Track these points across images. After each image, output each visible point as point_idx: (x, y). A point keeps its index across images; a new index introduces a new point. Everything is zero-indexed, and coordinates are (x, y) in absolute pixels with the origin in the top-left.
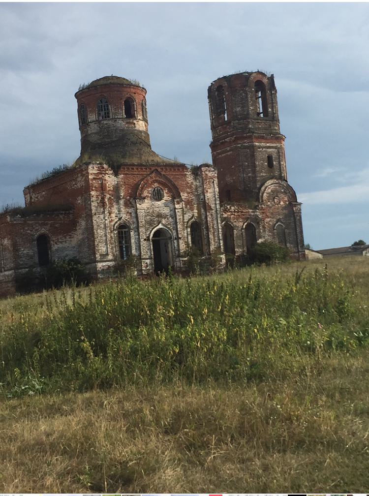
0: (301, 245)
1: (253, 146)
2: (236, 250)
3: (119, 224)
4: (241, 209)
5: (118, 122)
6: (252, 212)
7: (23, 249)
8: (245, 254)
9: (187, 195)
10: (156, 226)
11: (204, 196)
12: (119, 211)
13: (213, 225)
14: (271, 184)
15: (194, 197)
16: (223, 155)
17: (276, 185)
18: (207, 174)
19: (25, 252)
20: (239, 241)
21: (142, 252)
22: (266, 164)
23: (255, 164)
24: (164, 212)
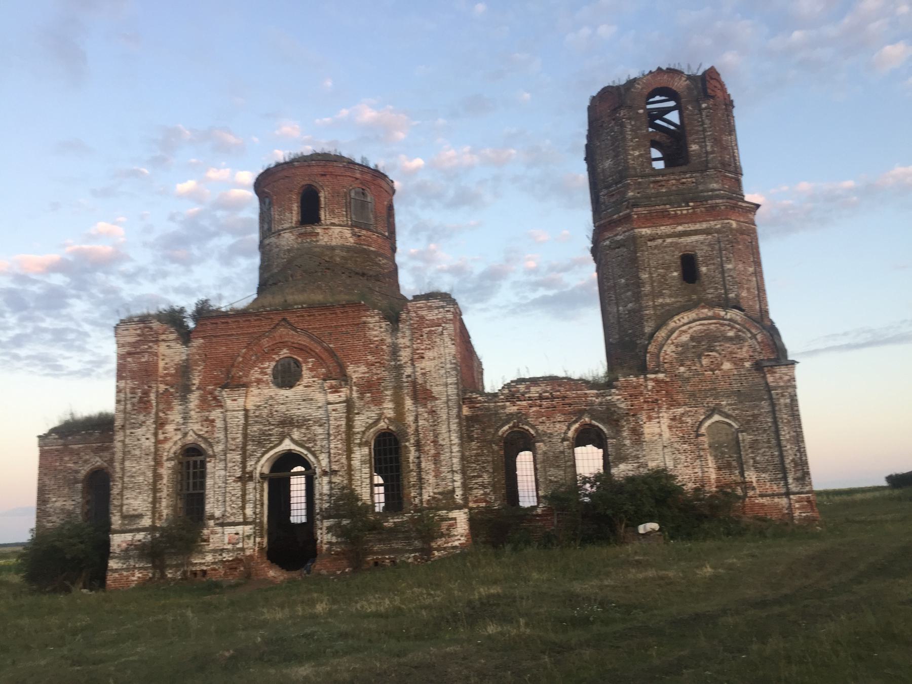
0: (799, 474)
3: (183, 447)
5: (284, 237)
6: (597, 396)
7: (54, 499)
9: (366, 370)
10: (272, 448)
12: (186, 418)
15: (386, 374)
18: (422, 318)
19: (58, 504)
23: (639, 278)
24: (298, 412)
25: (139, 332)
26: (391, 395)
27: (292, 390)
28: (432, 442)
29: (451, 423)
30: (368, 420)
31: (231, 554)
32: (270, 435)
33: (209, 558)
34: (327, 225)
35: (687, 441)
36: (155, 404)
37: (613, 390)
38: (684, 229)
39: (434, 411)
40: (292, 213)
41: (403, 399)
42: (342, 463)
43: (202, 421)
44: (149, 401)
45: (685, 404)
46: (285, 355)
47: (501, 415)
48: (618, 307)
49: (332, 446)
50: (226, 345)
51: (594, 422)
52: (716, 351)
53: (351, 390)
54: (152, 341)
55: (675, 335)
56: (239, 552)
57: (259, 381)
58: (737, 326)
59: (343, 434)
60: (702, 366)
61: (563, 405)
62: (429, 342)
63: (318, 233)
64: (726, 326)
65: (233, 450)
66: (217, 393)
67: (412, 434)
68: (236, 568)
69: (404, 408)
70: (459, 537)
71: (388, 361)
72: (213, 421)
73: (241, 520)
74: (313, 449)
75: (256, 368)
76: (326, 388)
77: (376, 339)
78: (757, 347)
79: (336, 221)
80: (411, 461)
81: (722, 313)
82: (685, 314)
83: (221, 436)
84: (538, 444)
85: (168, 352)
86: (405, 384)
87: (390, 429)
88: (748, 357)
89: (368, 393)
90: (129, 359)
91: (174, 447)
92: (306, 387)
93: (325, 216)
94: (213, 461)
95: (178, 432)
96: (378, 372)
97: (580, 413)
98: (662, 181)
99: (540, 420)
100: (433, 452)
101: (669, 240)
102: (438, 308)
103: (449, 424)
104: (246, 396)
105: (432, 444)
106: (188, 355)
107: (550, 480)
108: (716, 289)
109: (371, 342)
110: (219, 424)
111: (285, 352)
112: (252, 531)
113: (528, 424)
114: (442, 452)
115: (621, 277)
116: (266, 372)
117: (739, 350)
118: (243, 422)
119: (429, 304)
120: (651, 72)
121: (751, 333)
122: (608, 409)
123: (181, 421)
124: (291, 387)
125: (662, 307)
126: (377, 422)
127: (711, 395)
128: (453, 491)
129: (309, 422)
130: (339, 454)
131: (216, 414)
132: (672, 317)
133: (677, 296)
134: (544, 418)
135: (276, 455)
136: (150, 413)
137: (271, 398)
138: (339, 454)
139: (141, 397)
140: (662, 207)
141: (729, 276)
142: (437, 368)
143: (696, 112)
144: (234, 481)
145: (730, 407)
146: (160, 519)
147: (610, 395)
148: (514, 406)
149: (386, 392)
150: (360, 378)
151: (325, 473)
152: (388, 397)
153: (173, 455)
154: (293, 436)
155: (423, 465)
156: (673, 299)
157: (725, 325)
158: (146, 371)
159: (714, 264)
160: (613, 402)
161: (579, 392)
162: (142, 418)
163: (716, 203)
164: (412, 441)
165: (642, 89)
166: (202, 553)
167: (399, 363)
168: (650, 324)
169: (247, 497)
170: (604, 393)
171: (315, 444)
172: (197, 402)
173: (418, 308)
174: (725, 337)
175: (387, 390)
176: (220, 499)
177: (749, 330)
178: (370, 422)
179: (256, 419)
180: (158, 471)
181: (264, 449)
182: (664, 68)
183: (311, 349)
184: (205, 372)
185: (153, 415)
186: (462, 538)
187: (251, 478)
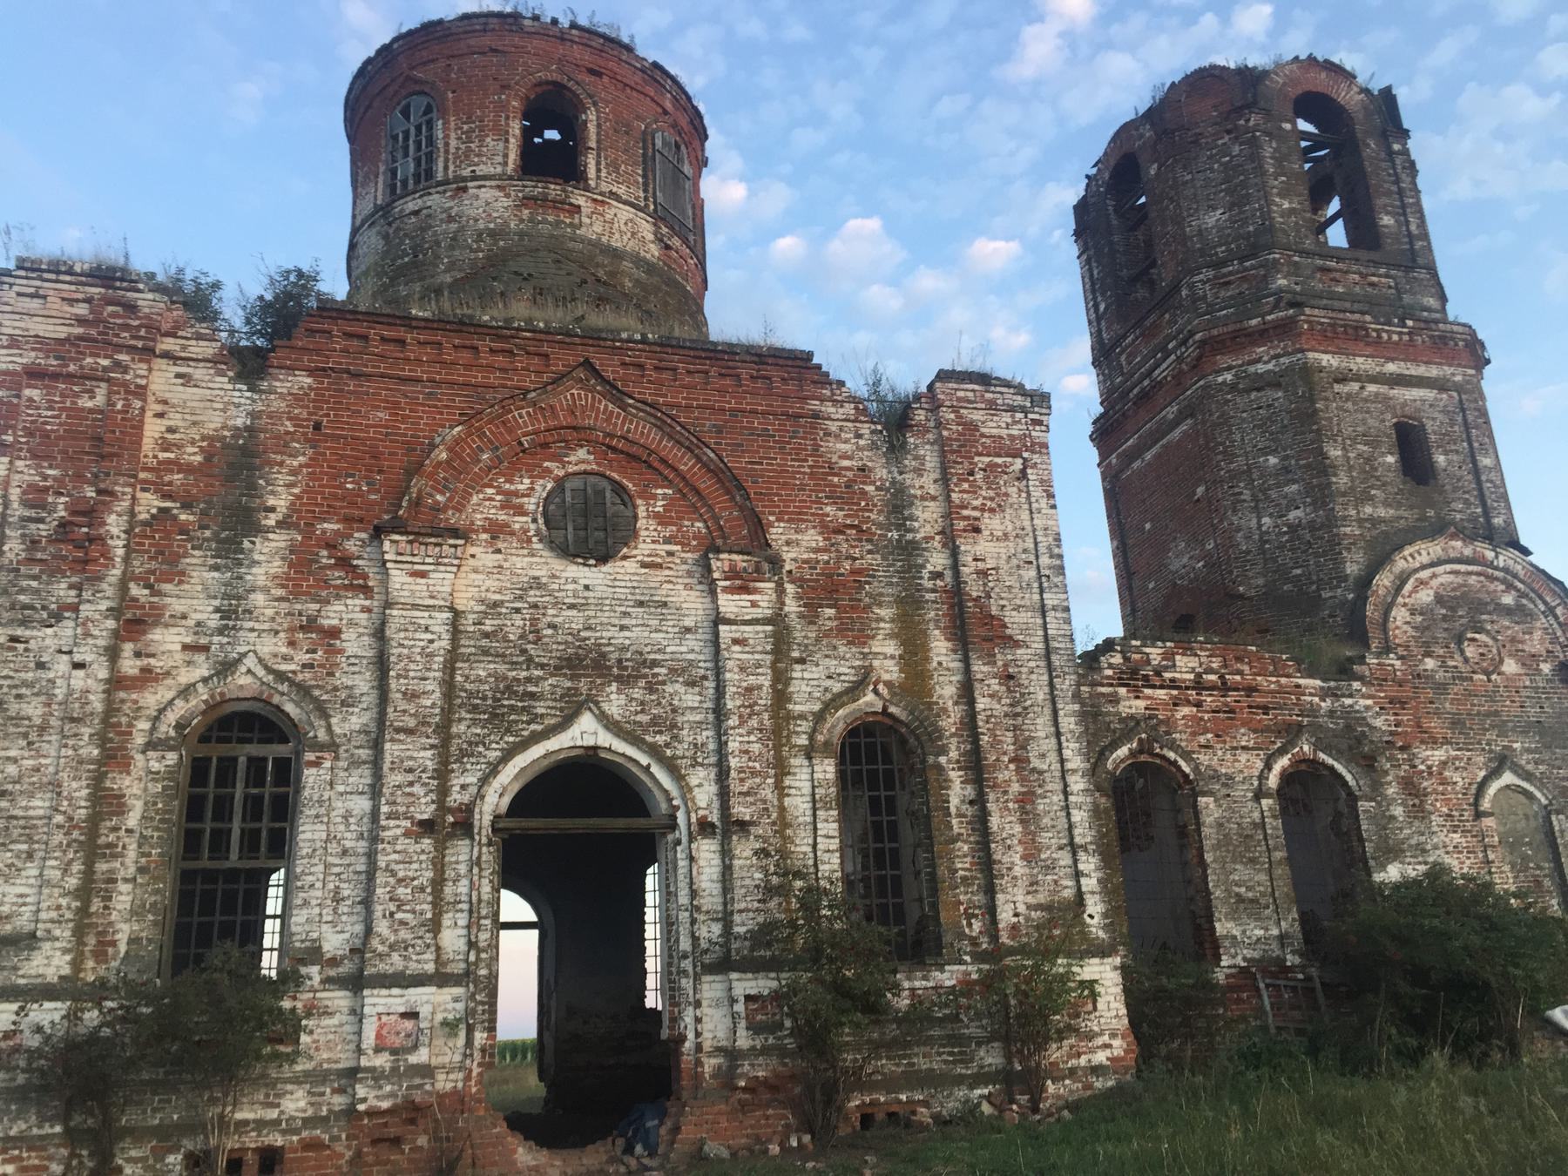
1: (1307, 372)
2: (1221, 928)
3: (211, 707)
4: (1243, 673)
8: (1291, 960)
10: (536, 738)
11: (955, 553)
12: (232, 613)
13: (1022, 744)
14: (1432, 565)
16: (1148, 456)
17: (1463, 568)
18: (972, 427)
20: (1241, 872)
21: (382, 927)
22: (1390, 459)
23: (1325, 456)
24: (621, 638)
25: (82, 310)
26: (892, 621)
27: (606, 568)
28: (1010, 761)
29: (1061, 713)
30: (829, 683)
31: (388, 1088)
32: (532, 696)
33: (296, 1103)
34: (601, 194)
35: (1458, 826)
36: (121, 552)
37: (1356, 685)
38: (1399, 371)
39: (1010, 677)
40: (507, 141)
41: (925, 633)
42: (765, 802)
43: (291, 630)
44: (100, 540)
45: (1446, 741)
46: (583, 467)
47: (1107, 719)
48: (1259, 518)
49: (733, 745)
50: (394, 407)
51: (1322, 756)
52: (1488, 633)
53: (780, 591)
54: (131, 349)
55: (1408, 587)
56: (417, 1081)
57: (496, 531)
58: (1520, 586)
59: (766, 716)
60: (1466, 660)
61: (1249, 707)
62: (991, 493)
63: (579, 207)
64: (1496, 583)
65: (410, 732)
66: (351, 546)
67: (953, 735)
68: (396, 1142)
69: (927, 659)
70: (1106, 1038)
71: (880, 526)
72: (335, 633)
73: (430, 968)
74: (669, 752)
75: (490, 491)
76: (716, 575)
77: (846, 463)
78: (1559, 633)
79: (621, 190)
80: (953, 810)
81: (1490, 555)
82: (1423, 546)
83: (363, 683)
84: (1202, 800)
85: (179, 394)
86: (930, 596)
87: (891, 716)
88: (1545, 654)
89: (830, 606)
90: (35, 394)
91: (179, 703)
92: (644, 565)
93: (599, 170)
94: (327, 764)
95: (200, 658)
96: (857, 552)
97: (1291, 733)
98: (1337, 271)
99: (1202, 740)
100: (1015, 788)
101: (1372, 388)
102: (1012, 409)
103: (1055, 712)
104: (459, 566)
105: (1012, 767)
106: (253, 415)
107: (1238, 895)
108: (1466, 502)
109: (833, 469)
110: (356, 644)
111: (581, 458)
112: (460, 1006)
113: (1173, 746)
114: (1040, 791)
115: (1266, 452)
116: (521, 506)
117: (1527, 637)
118: (445, 643)
119: (988, 396)
120: (1296, 58)
121: (1545, 603)
122: (1348, 727)
123: (214, 621)
124: (603, 559)
125: (1373, 525)
126: (855, 690)
127: (1493, 727)
128: (1080, 899)
129: (656, 670)
130: (754, 774)
131: (346, 612)
132: (1400, 548)
133: (1399, 505)
134: (1210, 736)
135: (546, 762)
136: (100, 579)
137: (536, 583)
138: (754, 774)
139: (63, 524)
140: (1357, 316)
141: (1487, 481)
142: (1015, 562)
143: (1383, 155)
144: (407, 834)
145: (1530, 757)
146: (100, 955)
147: (1351, 696)
148: (1137, 697)
149: (878, 611)
150: (805, 561)
151: (705, 828)
152: (882, 625)
153: (172, 733)
154: (605, 706)
155: (994, 822)
156: (1392, 512)
157: (1497, 579)
158: (100, 439)
159: (1457, 452)
160: (1358, 712)
161: (1283, 680)
162: (62, 590)
163: (1452, 332)
164: (954, 754)
165: (1284, 84)
166: (273, 1091)
167: (909, 536)
168: (1355, 557)
169: (448, 890)
170: (1337, 688)
171: (675, 738)
172: (277, 567)
173: (959, 399)
174: (1497, 604)
175: (880, 605)
176: (346, 893)
177: (1541, 597)
178: (835, 690)
179: (484, 642)
180: (108, 784)
181: (511, 739)
182: (1320, 59)
183: (664, 461)
184: (312, 476)
185: (108, 587)
186: (1117, 1043)
187: (464, 826)
